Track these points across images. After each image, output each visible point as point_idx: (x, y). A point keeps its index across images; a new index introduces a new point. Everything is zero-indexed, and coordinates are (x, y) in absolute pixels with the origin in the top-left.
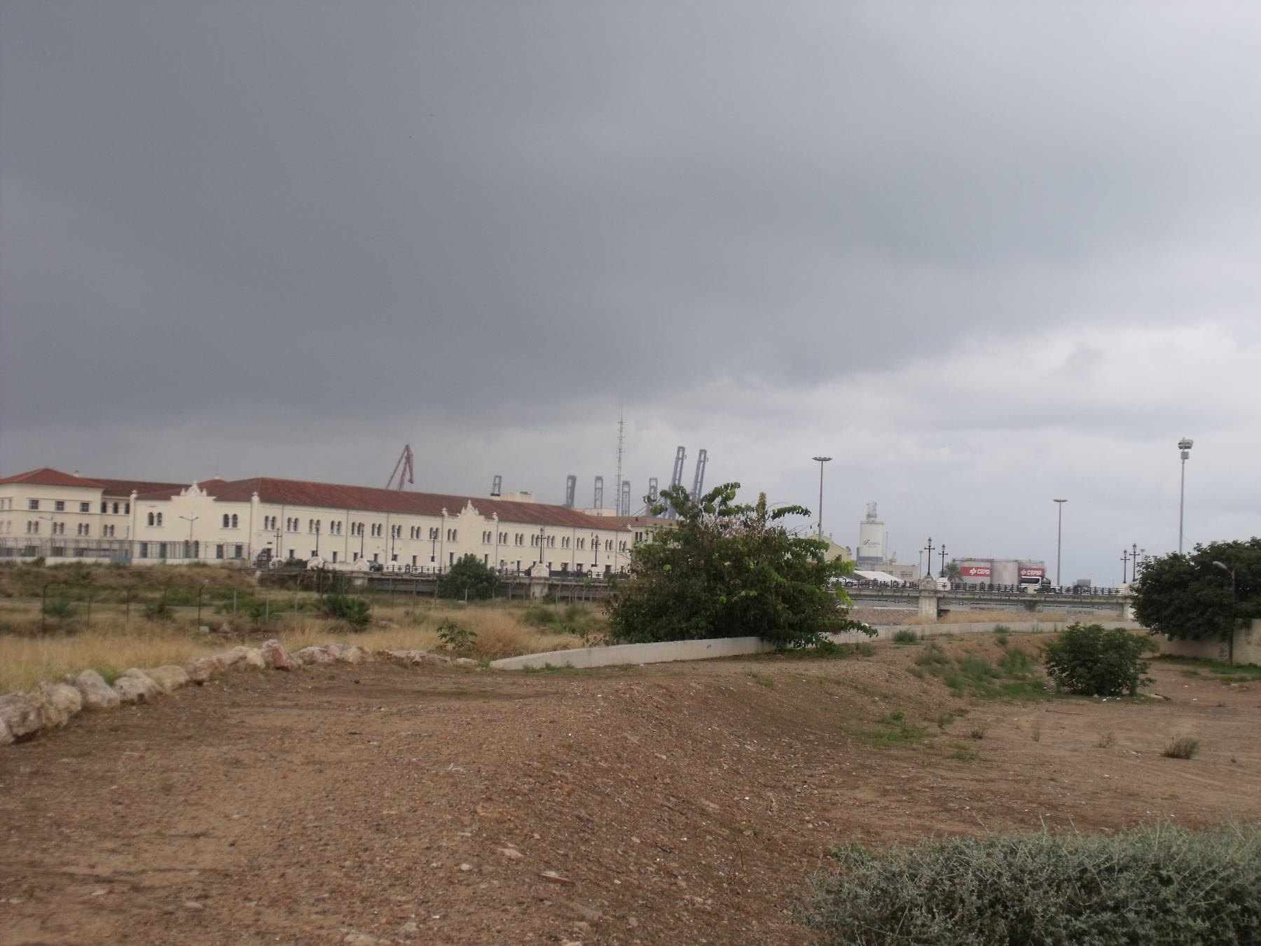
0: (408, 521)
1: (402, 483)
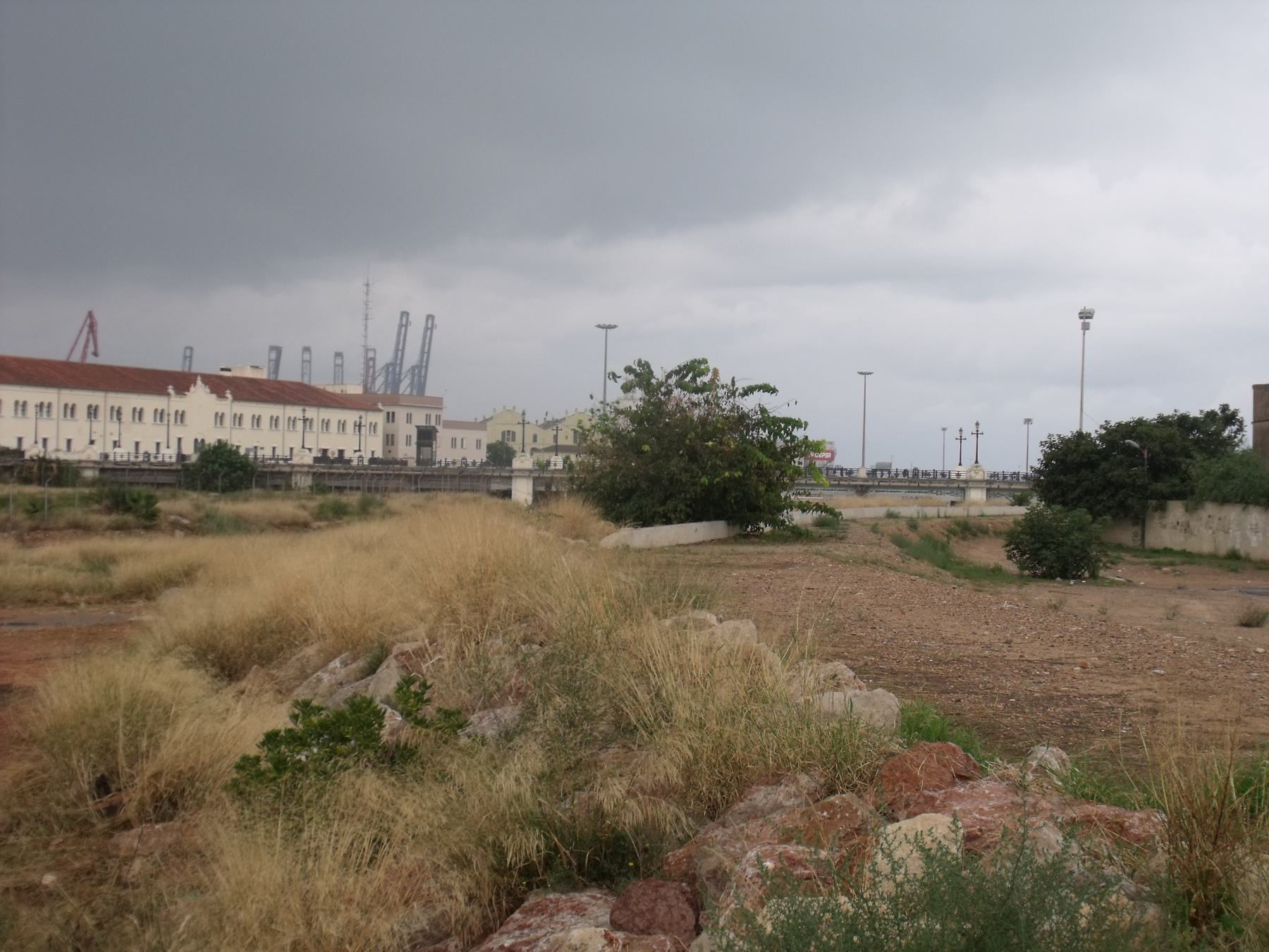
0: (128, 402)
1: (84, 355)
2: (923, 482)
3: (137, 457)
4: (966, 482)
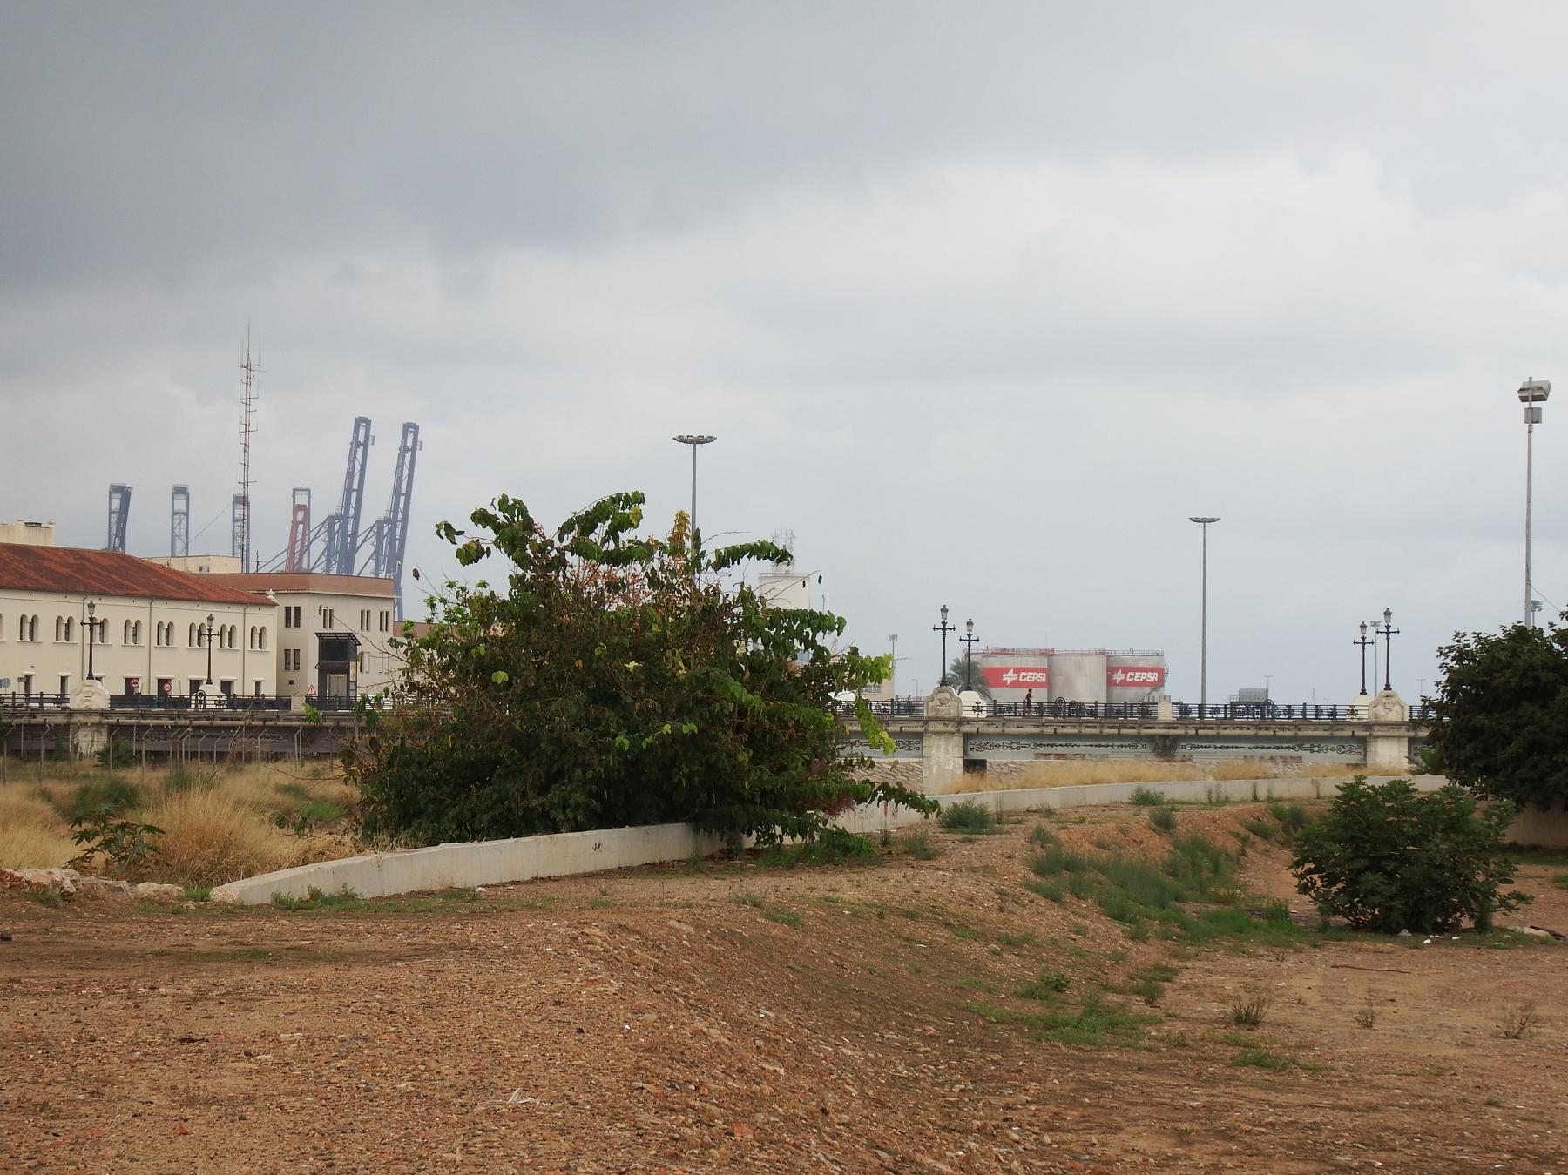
2: (1282, 727)
4: (1368, 726)
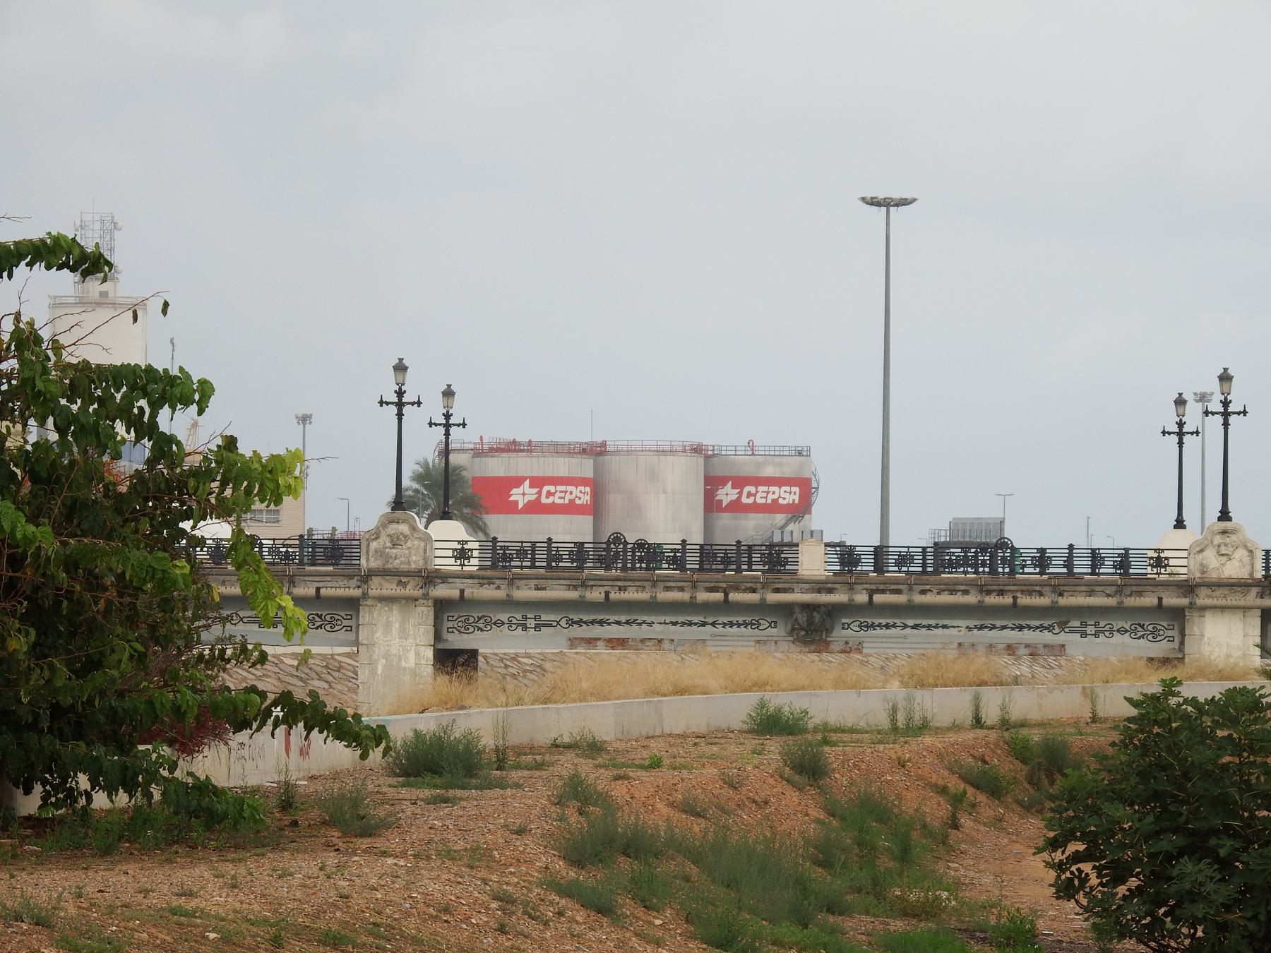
2: (1029, 589)
3: (964, 537)
4: (1188, 588)
